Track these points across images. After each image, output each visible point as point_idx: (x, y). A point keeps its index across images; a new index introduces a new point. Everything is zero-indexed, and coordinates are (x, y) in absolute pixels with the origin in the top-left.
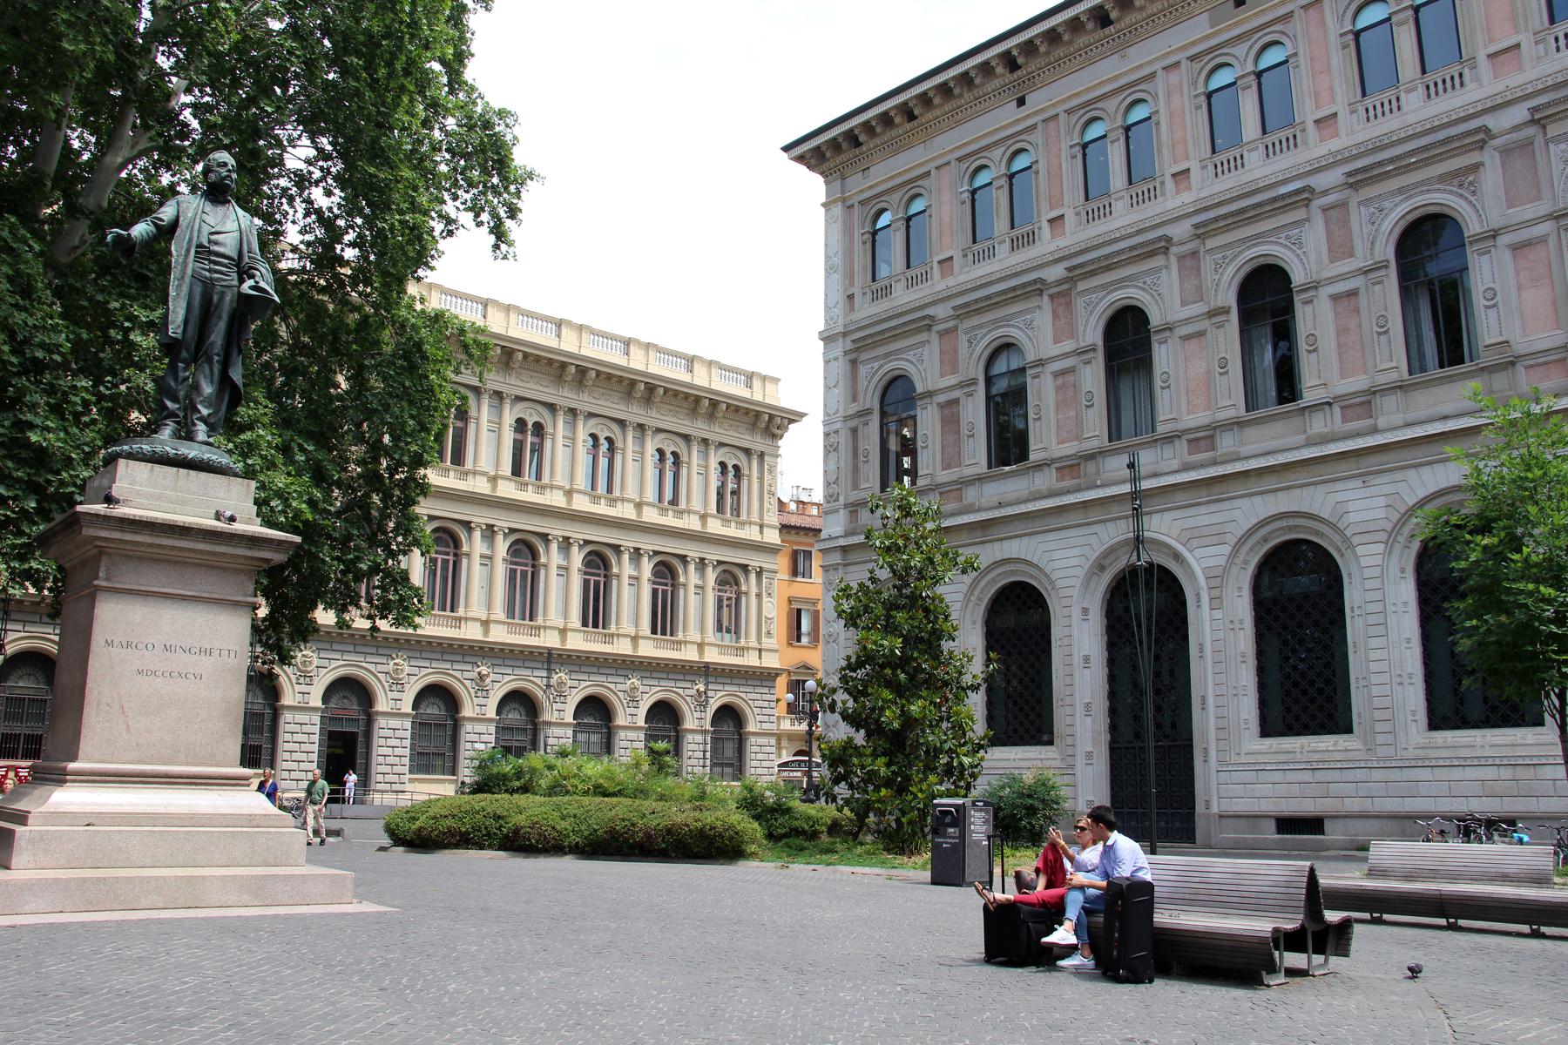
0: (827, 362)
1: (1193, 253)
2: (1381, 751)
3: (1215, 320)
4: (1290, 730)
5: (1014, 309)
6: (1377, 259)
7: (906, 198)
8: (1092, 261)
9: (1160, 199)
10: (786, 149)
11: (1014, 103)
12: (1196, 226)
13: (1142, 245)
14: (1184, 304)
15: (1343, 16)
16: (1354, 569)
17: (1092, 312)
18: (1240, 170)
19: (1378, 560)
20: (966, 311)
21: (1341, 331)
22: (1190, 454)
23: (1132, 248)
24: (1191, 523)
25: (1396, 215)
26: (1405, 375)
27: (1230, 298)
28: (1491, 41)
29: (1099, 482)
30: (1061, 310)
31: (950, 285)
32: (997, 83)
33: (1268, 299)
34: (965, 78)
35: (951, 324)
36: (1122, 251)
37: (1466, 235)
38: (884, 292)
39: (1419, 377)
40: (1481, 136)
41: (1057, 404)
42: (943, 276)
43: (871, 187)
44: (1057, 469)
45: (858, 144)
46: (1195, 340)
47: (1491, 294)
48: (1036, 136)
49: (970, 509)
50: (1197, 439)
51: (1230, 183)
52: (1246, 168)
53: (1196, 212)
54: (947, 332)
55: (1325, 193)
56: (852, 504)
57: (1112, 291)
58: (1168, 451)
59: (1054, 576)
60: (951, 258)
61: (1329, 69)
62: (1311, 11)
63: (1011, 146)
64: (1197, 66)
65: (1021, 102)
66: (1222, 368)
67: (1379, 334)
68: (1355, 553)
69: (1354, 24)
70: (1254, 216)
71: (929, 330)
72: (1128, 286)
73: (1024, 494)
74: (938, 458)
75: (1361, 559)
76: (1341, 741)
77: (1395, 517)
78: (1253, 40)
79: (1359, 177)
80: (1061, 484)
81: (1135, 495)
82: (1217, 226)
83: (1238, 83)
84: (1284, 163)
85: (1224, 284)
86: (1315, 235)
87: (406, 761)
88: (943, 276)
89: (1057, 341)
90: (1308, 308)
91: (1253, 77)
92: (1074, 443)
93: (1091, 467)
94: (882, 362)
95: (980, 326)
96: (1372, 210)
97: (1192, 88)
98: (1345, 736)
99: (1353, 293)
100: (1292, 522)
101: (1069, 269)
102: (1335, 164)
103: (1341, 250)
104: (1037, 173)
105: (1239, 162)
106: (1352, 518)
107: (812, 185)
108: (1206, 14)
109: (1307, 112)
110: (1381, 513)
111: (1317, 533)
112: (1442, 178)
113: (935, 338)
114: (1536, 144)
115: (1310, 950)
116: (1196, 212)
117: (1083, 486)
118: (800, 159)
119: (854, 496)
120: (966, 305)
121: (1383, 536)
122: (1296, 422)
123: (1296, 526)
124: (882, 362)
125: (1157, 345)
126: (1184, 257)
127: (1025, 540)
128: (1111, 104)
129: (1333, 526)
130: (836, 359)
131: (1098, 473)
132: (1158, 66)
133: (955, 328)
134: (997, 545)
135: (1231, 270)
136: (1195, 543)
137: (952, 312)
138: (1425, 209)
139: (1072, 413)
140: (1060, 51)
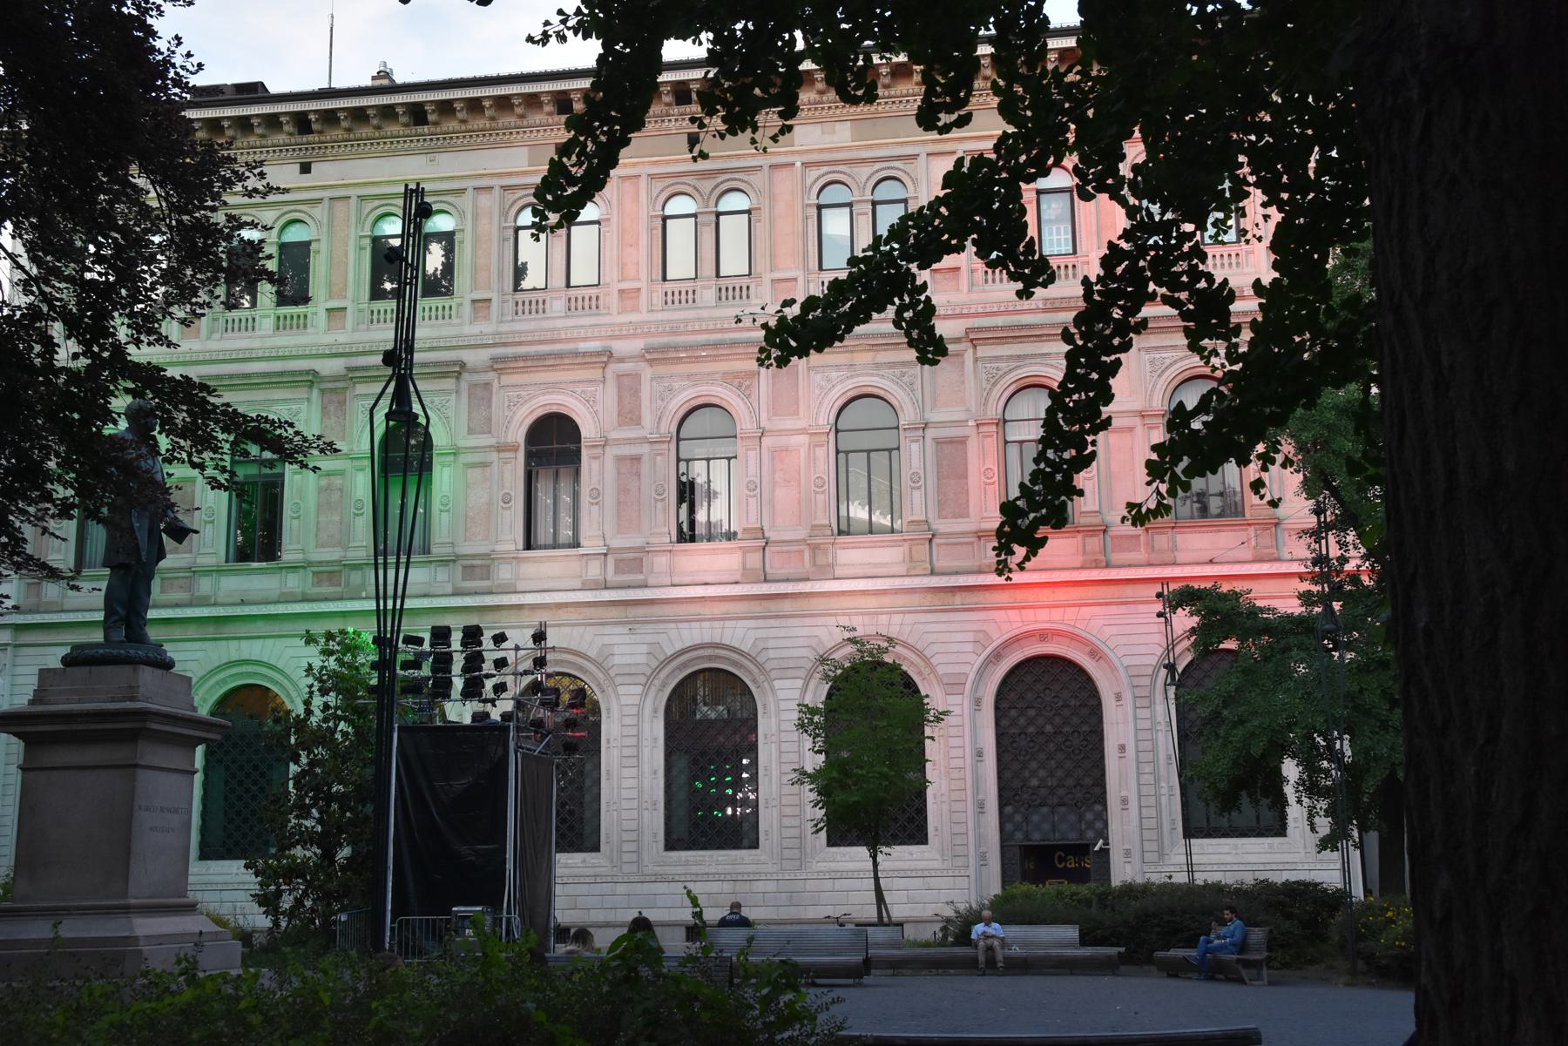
1: (486, 384)
2: (627, 869)
3: (503, 455)
4: (832, 846)
9: (455, 321)
11: (297, 167)
13: (436, 364)
14: (471, 431)
15: (656, 199)
17: (994, 384)
18: (541, 315)
19: (636, 700)
21: (622, 490)
27: (518, 435)
29: (364, 594)
30: (332, 408)
31: (485, 331)
32: (281, 138)
33: (555, 446)
38: (288, 322)
41: (319, 505)
42: (280, 325)
44: (314, 573)
46: (479, 470)
48: (319, 212)
49: (204, 602)
50: (473, 566)
55: (622, 360)
58: (442, 574)
59: (768, 667)
60: (795, 279)
61: (638, 244)
62: (627, 183)
63: (286, 213)
65: (306, 169)
66: (505, 503)
68: (615, 691)
69: (515, 221)
70: (553, 366)
73: (274, 595)
75: (621, 697)
76: (589, 857)
77: (655, 664)
79: (655, 356)
80: (317, 590)
82: (516, 365)
86: (607, 397)
88: (475, 319)
92: (336, 549)
97: (503, 219)
98: (593, 854)
99: (636, 459)
100: (709, 652)
101: (349, 369)
102: (961, 316)
103: (630, 416)
105: (690, 296)
106: (617, 660)
108: (849, 123)
110: (642, 659)
116: (494, 345)
117: (345, 596)
121: (643, 679)
123: (562, 661)
125: (439, 467)
126: (476, 385)
127: (270, 642)
129: (753, 660)
134: (233, 644)
138: (708, 398)
139: (337, 518)
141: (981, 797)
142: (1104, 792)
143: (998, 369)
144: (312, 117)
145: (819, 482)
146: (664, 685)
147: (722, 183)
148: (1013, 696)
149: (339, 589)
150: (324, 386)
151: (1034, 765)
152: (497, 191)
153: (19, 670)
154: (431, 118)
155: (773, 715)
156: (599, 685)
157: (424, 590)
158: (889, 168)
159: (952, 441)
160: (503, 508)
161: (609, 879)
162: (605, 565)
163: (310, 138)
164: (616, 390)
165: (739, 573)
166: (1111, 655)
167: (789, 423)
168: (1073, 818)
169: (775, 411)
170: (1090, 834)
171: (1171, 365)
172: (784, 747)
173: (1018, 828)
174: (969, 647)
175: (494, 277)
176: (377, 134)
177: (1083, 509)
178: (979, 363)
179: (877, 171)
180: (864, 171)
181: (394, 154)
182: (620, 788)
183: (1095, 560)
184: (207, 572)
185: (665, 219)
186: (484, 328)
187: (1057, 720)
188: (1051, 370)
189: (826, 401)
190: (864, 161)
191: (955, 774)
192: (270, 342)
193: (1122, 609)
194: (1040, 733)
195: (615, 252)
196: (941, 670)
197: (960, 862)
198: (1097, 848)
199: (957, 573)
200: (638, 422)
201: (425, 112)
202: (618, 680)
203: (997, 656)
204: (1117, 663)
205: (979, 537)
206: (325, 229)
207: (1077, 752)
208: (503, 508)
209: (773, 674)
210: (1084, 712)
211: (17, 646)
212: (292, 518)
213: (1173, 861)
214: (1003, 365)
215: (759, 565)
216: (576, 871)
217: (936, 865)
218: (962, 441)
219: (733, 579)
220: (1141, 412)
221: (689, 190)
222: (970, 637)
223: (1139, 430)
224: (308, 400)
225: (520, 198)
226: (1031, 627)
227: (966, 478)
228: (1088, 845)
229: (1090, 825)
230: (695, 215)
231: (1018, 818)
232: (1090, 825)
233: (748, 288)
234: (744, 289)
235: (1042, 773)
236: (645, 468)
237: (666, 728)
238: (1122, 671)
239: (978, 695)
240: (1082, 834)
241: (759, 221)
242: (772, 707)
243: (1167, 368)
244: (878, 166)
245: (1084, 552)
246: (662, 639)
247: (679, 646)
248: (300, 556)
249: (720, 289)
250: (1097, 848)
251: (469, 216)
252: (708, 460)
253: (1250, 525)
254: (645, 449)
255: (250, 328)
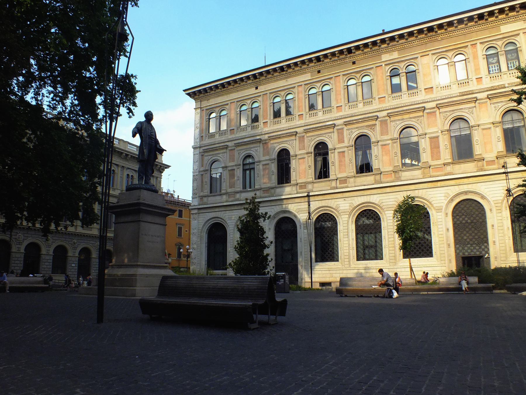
0: (194, 155)
2: (346, 266)
3: (308, 155)
4: (365, 259)
5: (252, 146)
6: (350, 144)
7: (221, 110)
8: (276, 136)
9: (294, 121)
10: (184, 91)
11: (317, 72)
12: (304, 130)
14: (300, 150)
16: (385, 217)
17: (446, 119)
19: (347, 219)
20: (238, 145)
21: (340, 161)
22: (300, 189)
23: (287, 133)
24: (299, 207)
25: (356, 133)
26: (242, 190)
28: (337, 103)
34: (205, 90)
35: (233, 148)
36: (284, 134)
37: (371, 141)
39: (245, 190)
40: (376, 118)
43: (210, 105)
44: (263, 191)
45: (207, 92)
47: (376, 156)
50: (302, 186)
51: (313, 120)
52: (318, 116)
53: (305, 126)
54: (232, 150)
55: (338, 126)
56: (201, 196)
57: (280, 144)
58: (294, 188)
60: (234, 129)
64: (307, 87)
65: (257, 88)
67: (309, 169)
69: (308, 93)
71: (226, 149)
72: (285, 143)
74: (228, 184)
78: (406, 63)
80: (264, 195)
81: (308, 196)
83: (317, 93)
84: (328, 116)
85: (311, 146)
86: (335, 136)
87: (51, 270)
88: (299, 119)
89: (264, 156)
90: (333, 155)
91: (321, 92)
93: (273, 191)
94: (212, 156)
95: (242, 150)
96: (349, 132)
98: (337, 262)
99: (344, 152)
100: (366, 204)
102: (341, 119)
104: (260, 109)
106: (341, 208)
107: (191, 103)
108: (310, 73)
109: (334, 104)
110: (348, 208)
111: (333, 212)
112: (367, 126)
113: (228, 151)
114: (388, 121)
115: (270, 314)
116: (305, 126)
118: (189, 94)
119: (202, 194)
120: (238, 143)
122: (328, 183)
124: (212, 156)
128: (282, 93)
130: (197, 154)
131: (275, 193)
132: (296, 85)
133: (234, 149)
135: (313, 142)
136: (300, 212)
137: (234, 145)
140: (270, 76)
141: (449, 243)
142: (488, 240)
143: (447, 115)
144: (257, 75)
145: (294, 168)
146: (354, 214)
147: (362, 74)
148: (457, 212)
149: (269, 194)
150: (230, 149)
151: (465, 232)
152: (303, 86)
153: (199, 219)
154: (353, 51)
155: (386, 222)
156: (336, 215)
157: (289, 193)
158: (490, 44)
159: (434, 138)
160: (395, 156)
161: (341, 269)
162: (337, 182)
163: (257, 80)
164: (337, 134)
165: (374, 181)
166: (488, 197)
167: (385, 137)
168: (477, 248)
169: (382, 134)
170: (483, 252)
171: (501, 107)
172: (389, 230)
173: (461, 251)
174: (443, 198)
175: (304, 108)
176: (416, 39)
177: (476, 154)
178: (441, 114)
179: (391, 67)
180: (249, 101)
181: (277, 80)
182: (343, 244)
183: (481, 169)
184: (238, 192)
185: (348, 86)
186: (302, 122)
187: (472, 219)
188: (464, 113)
189: (396, 130)
190: (402, 61)
191: (441, 236)
192: (363, 110)
193: (491, 183)
194: (467, 222)
195: (335, 96)
196: (435, 205)
197: (443, 262)
198: (486, 257)
199: (438, 176)
200: (343, 142)
201: (284, 68)
202: (342, 214)
203: (452, 200)
204: (490, 200)
205: (444, 165)
206: (334, 85)
207: (478, 228)
208: (395, 156)
209: (385, 210)
210: (480, 215)
211: (198, 213)
212: (293, 172)
213: (511, 260)
214: (398, 122)
215: (379, 179)
216: (333, 267)
217: (435, 263)
218: (437, 137)
219: (372, 183)
220: (493, 122)
221: (354, 77)
222: (443, 195)
223: (493, 128)
224: (260, 146)
225: (309, 86)
226: (462, 191)
227: (439, 148)
228: (483, 256)
229: (483, 250)
230: (356, 84)
231: (461, 248)
232: (483, 250)
233: (372, 101)
234: (371, 102)
235: (468, 235)
236: (346, 154)
237: (356, 227)
238: (492, 202)
239: (447, 212)
240: (481, 253)
241: (373, 83)
242: (385, 219)
243: (500, 108)
244: (391, 65)
245: (478, 167)
246: (353, 202)
247: (358, 203)
248: (259, 187)
249: (364, 103)
250: (486, 257)
251: (296, 94)
252: (216, 174)
253: (475, 161)
254: (346, 149)
255: (330, 112)
